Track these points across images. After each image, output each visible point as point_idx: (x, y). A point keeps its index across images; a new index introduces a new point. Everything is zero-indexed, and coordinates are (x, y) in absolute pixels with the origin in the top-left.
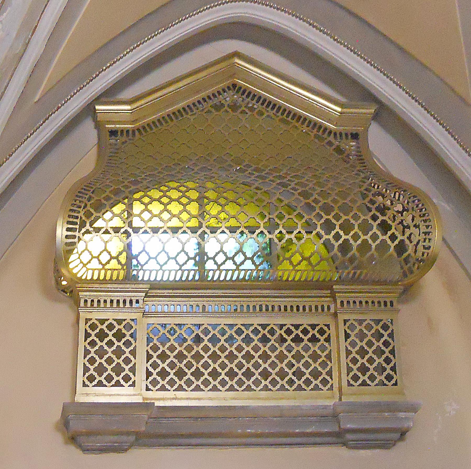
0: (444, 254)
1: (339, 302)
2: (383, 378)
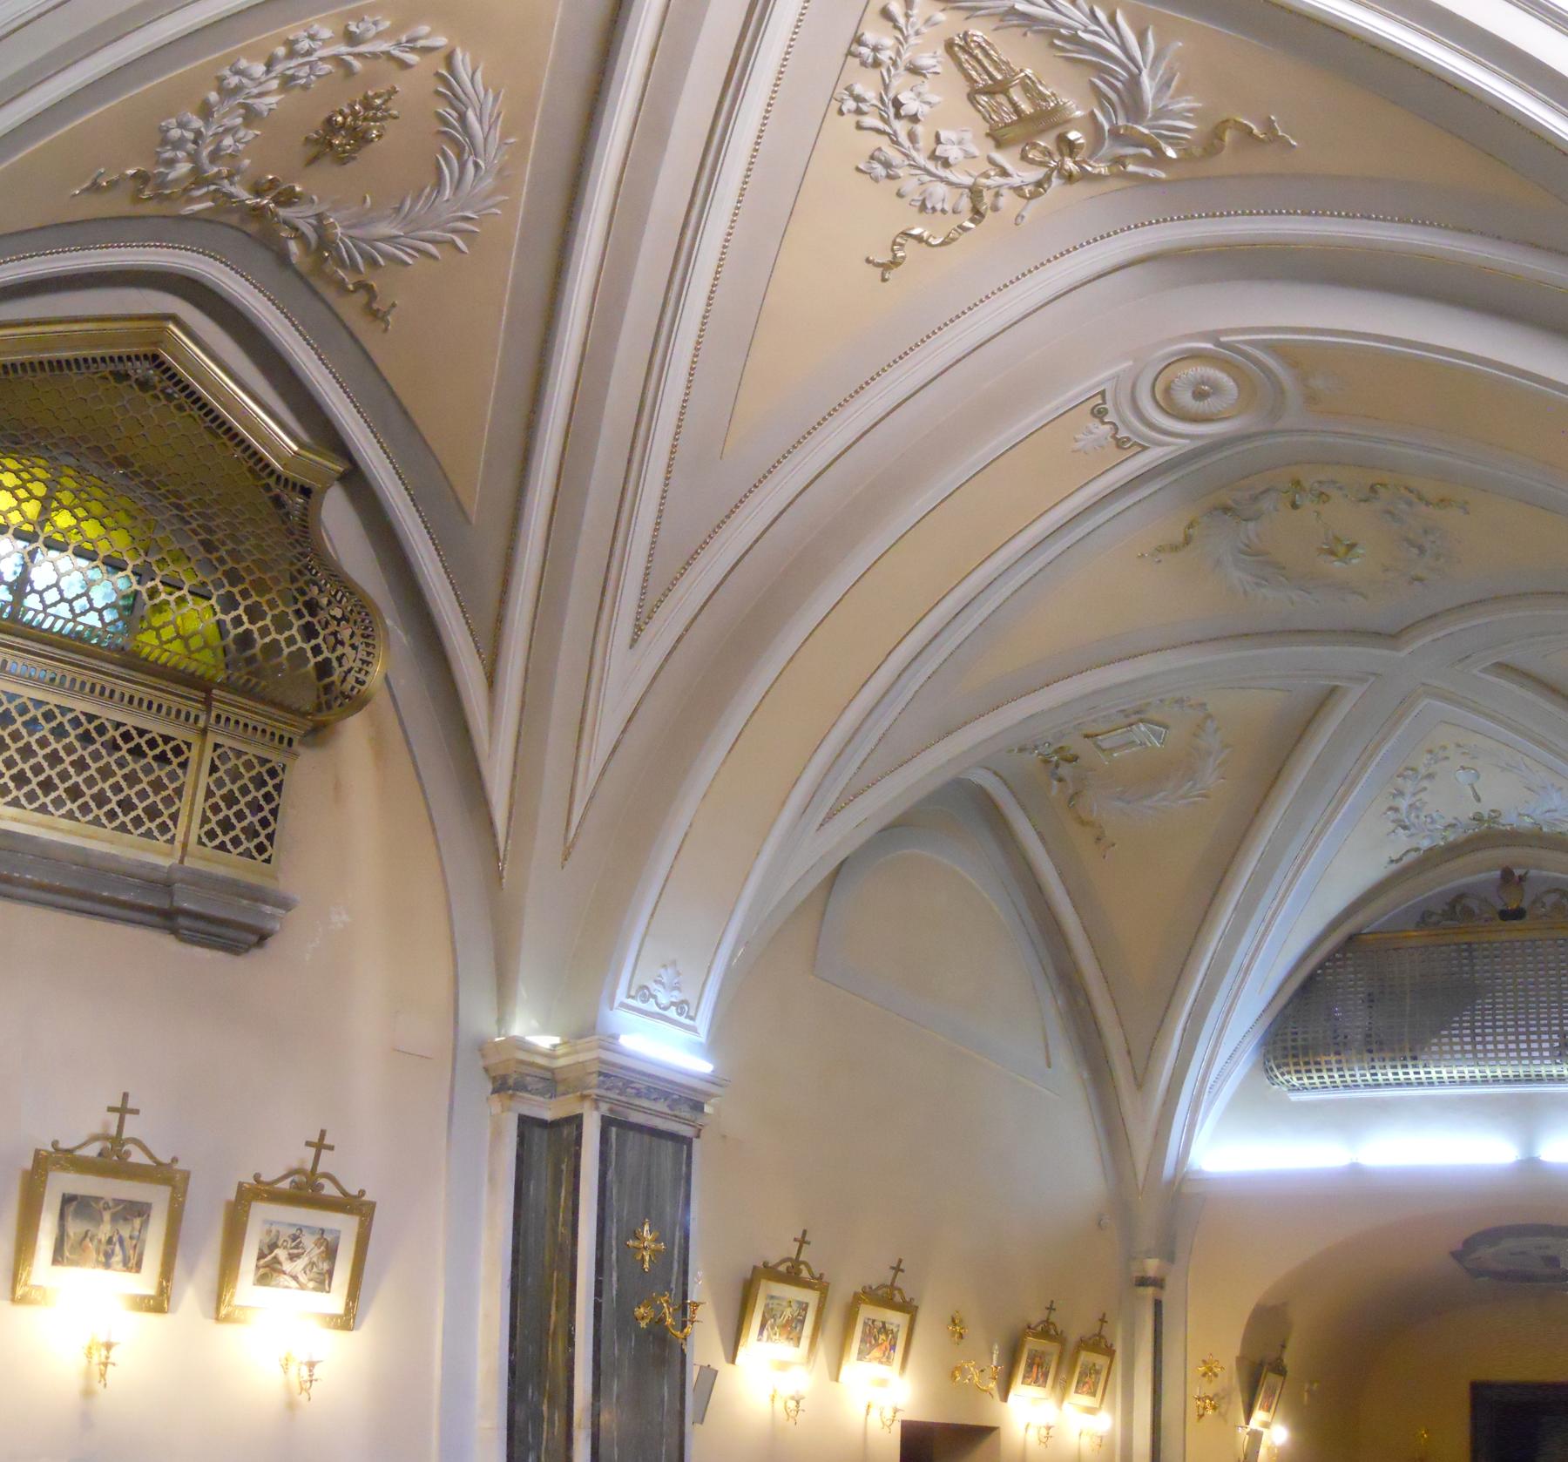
0: (381, 699)
1: (213, 714)
2: (252, 845)
